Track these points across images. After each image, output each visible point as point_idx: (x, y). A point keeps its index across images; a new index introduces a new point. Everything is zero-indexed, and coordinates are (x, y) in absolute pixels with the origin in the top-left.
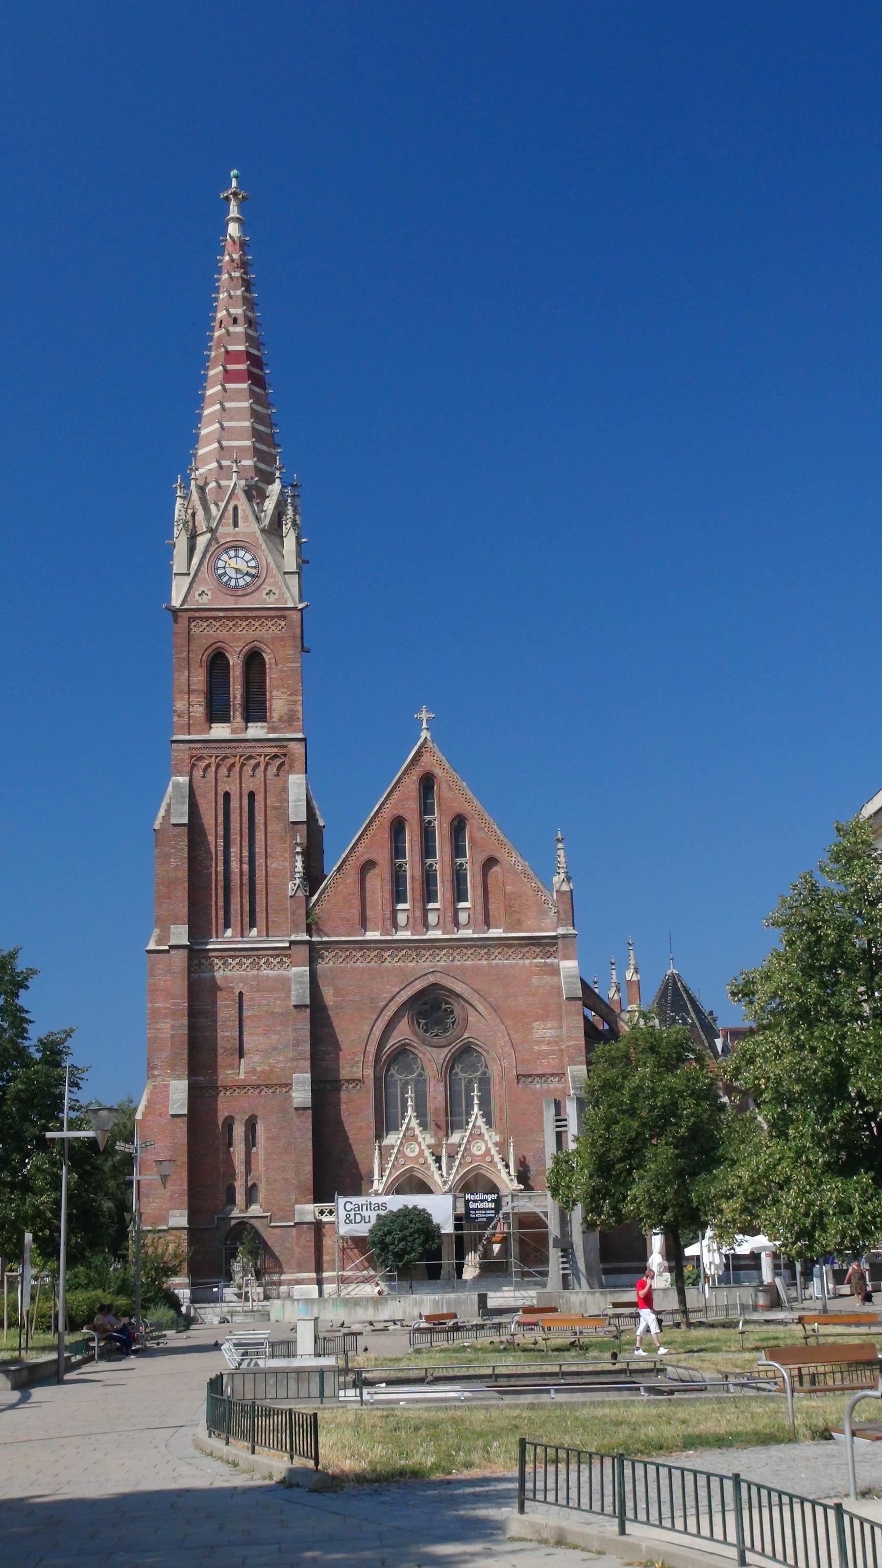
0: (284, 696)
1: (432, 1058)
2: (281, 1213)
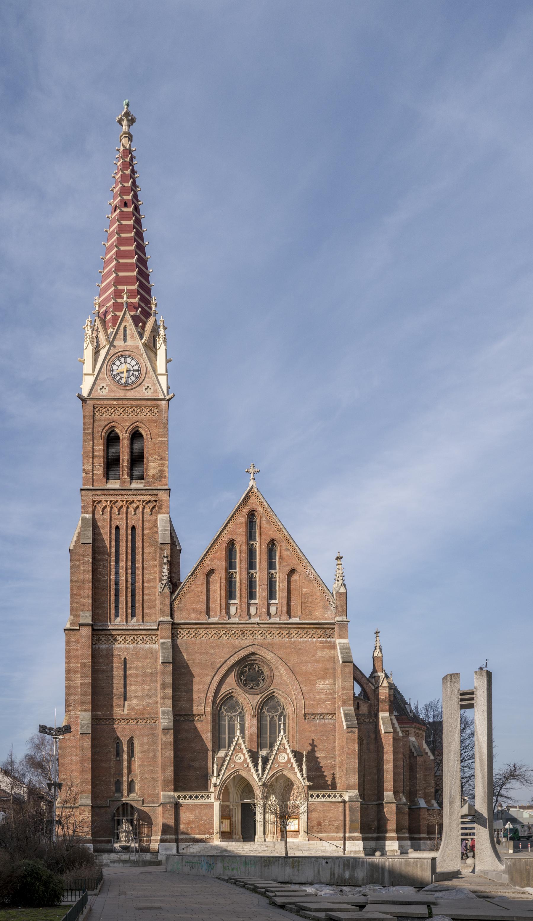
0: (156, 461)
1: (248, 701)
2: (150, 799)
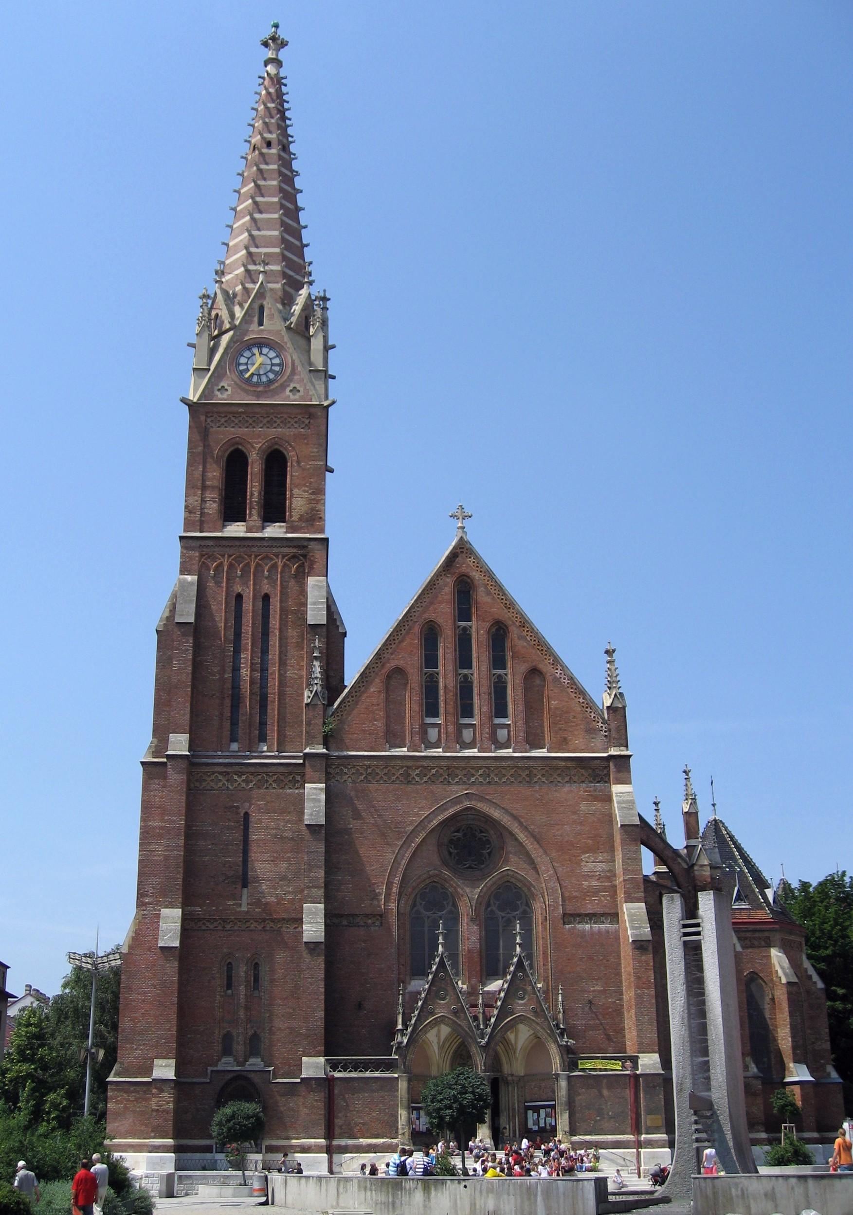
0: (306, 495)
